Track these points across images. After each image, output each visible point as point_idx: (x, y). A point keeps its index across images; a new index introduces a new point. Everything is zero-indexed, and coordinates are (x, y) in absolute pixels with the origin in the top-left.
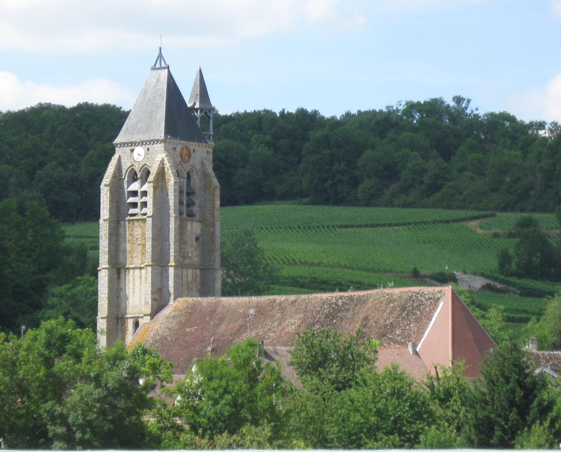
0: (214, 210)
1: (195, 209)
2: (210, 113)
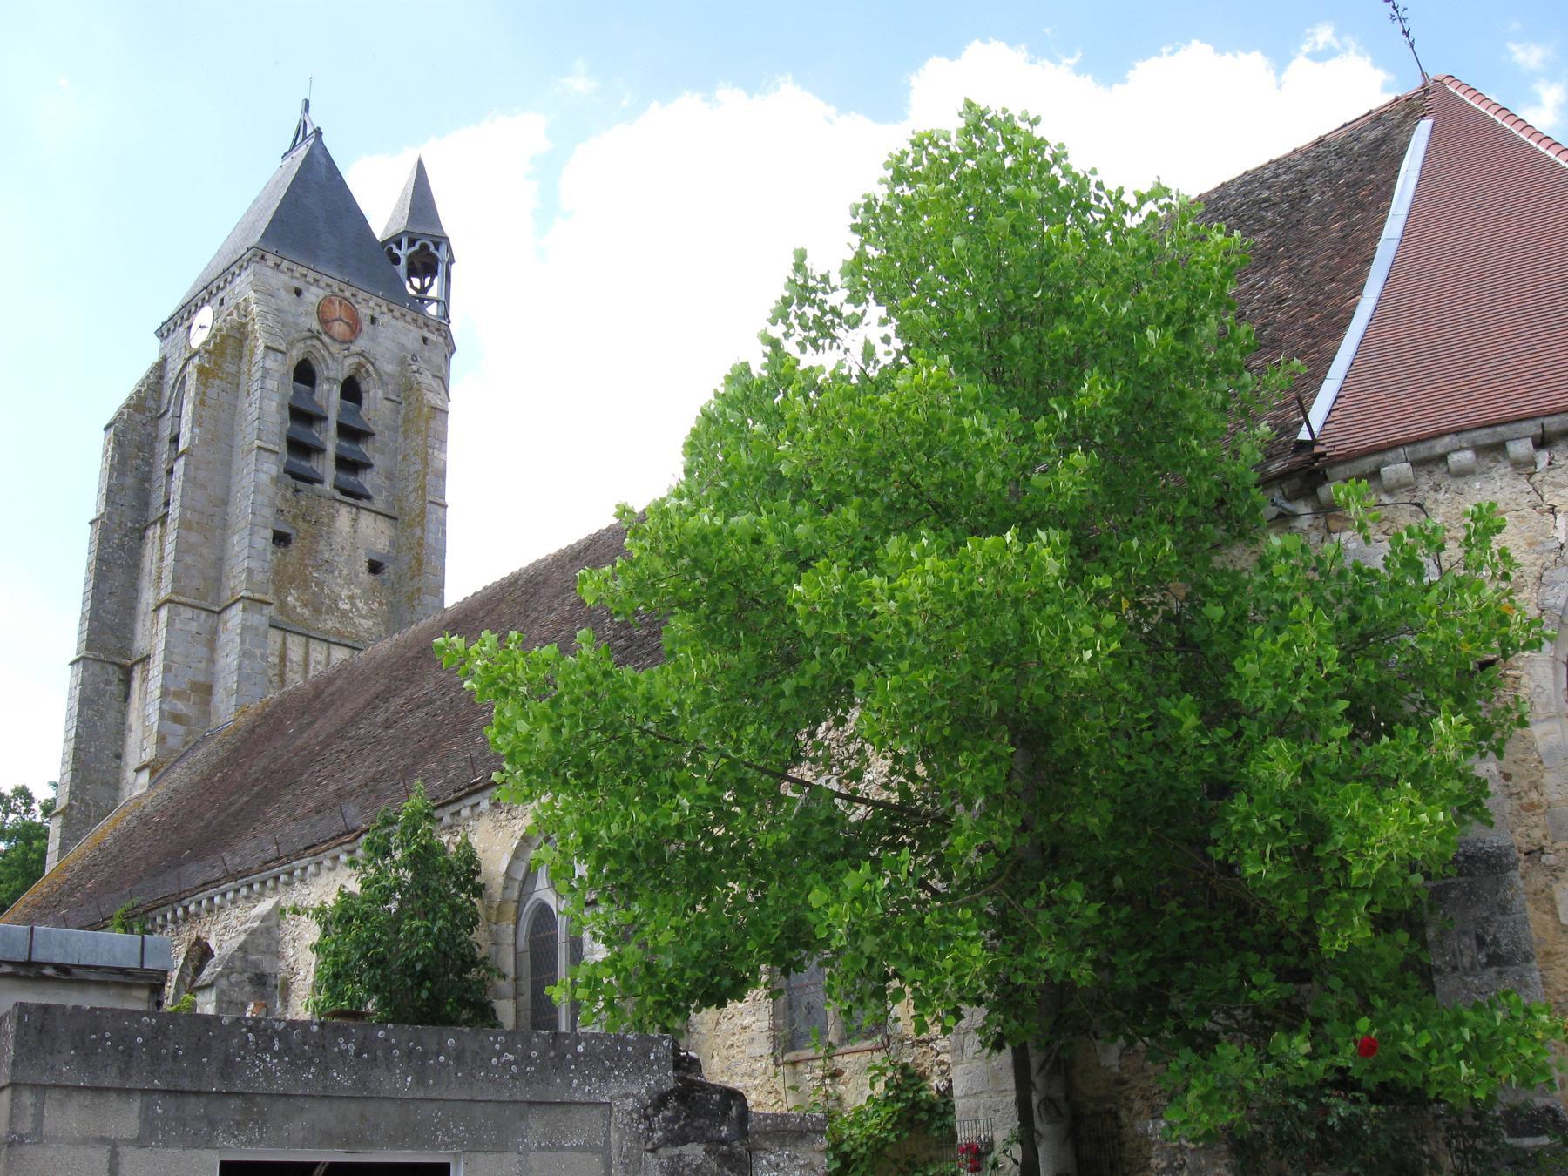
0: (426, 474)
1: (368, 480)
2: (437, 248)
